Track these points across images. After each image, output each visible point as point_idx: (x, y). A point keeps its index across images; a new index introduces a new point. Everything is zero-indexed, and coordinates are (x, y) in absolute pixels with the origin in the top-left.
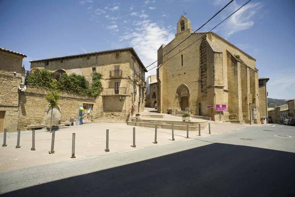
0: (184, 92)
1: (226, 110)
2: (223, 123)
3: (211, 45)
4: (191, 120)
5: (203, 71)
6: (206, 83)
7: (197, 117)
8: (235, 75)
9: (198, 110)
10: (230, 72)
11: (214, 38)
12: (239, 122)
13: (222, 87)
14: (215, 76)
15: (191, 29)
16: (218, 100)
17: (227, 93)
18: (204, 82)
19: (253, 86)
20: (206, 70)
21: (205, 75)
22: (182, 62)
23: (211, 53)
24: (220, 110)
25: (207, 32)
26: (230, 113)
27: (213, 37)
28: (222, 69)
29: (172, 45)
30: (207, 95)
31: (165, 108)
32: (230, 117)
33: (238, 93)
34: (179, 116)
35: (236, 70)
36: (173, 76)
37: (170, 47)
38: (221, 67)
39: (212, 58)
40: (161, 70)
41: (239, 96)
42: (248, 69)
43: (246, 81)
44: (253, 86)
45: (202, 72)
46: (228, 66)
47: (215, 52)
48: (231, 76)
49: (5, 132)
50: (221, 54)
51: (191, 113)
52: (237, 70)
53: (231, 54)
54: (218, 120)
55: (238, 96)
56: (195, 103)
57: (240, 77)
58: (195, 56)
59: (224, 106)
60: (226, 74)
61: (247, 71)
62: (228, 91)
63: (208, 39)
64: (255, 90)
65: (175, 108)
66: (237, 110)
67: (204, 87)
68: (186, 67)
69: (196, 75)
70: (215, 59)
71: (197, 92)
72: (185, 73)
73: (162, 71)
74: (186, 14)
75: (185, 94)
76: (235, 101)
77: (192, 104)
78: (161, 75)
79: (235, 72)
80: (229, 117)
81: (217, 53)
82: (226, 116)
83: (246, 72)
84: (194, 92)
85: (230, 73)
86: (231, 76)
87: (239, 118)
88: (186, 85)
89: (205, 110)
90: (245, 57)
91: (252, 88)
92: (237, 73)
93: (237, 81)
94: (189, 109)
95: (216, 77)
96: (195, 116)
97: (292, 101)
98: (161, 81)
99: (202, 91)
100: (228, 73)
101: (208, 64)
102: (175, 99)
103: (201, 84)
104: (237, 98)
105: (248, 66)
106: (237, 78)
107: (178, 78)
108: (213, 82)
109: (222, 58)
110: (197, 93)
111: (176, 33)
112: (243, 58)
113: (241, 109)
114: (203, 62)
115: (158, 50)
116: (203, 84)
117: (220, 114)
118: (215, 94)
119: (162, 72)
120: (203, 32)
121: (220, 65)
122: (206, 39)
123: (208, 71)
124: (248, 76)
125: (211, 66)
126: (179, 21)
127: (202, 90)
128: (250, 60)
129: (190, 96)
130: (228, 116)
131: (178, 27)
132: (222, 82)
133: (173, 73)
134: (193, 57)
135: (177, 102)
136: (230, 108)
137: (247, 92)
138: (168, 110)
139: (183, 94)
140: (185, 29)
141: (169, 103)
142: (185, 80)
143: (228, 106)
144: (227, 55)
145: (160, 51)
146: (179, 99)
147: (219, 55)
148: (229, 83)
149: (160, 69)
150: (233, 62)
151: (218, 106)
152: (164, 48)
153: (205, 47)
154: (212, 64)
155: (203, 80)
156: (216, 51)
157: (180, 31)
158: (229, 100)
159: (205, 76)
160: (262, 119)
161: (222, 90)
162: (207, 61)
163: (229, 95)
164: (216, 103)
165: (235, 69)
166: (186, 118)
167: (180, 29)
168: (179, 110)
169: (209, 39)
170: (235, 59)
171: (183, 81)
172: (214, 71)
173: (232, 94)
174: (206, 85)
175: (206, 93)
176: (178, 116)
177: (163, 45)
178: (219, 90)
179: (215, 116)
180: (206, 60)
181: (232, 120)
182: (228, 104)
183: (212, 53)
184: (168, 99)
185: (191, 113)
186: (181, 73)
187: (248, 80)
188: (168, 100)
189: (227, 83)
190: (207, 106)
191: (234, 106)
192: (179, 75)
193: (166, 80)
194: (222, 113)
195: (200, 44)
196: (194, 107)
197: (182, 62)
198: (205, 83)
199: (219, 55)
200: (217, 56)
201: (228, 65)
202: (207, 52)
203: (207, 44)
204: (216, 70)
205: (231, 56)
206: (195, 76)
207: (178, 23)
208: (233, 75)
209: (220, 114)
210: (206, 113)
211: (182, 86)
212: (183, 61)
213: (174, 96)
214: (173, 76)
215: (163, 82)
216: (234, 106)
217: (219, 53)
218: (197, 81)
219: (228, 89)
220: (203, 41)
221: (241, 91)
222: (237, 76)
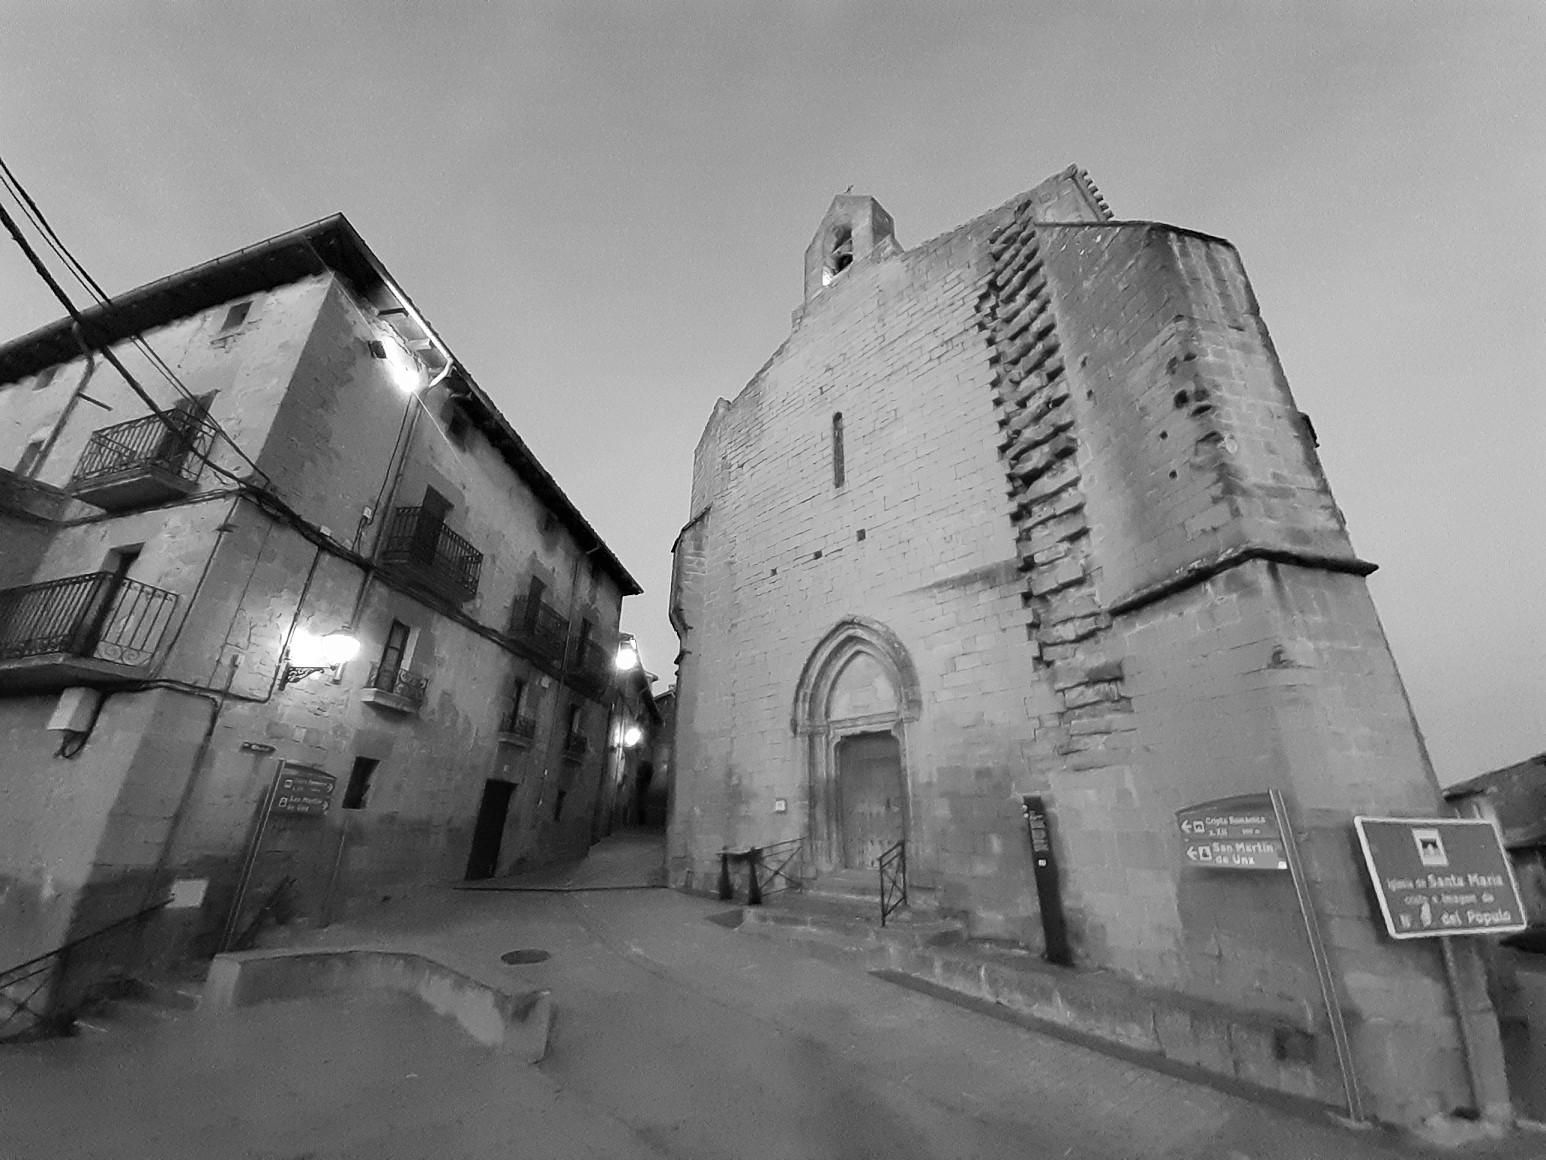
192: (818, 555)
200: (1191, 273)
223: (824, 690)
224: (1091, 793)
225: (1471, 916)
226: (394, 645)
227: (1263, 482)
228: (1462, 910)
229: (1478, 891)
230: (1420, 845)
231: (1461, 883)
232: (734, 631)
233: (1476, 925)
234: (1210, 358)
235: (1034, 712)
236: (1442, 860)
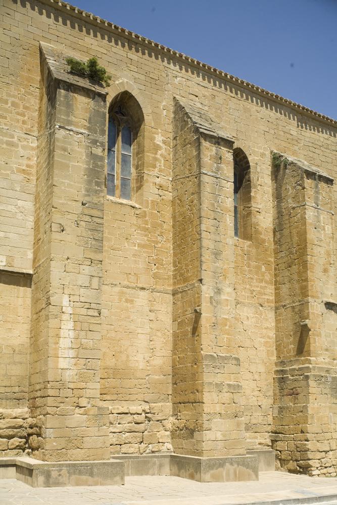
64: (306, 280)
91: (295, 268)
137: (201, 280)
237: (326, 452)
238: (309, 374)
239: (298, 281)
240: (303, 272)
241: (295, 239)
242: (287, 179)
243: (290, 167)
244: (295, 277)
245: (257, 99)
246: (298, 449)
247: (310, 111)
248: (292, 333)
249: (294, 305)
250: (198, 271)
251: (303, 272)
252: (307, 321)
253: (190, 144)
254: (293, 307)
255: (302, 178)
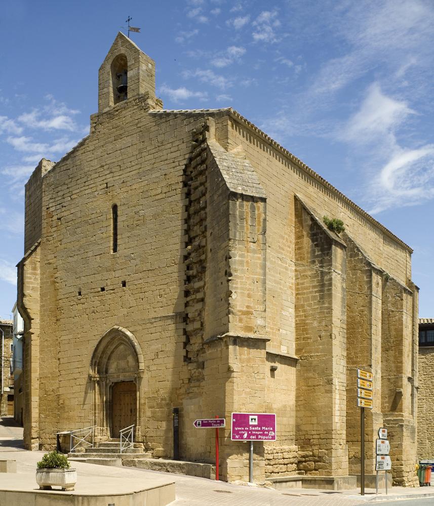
0: (123, 364)
1: (273, 438)
2: (262, 490)
3: (222, 165)
4: (72, 485)
5: (191, 272)
6: (202, 324)
7: (164, 464)
8: (322, 297)
9: (171, 434)
10: (306, 285)
11: (241, 137)
12: (330, 482)
13: (258, 343)
14: (234, 296)
15: (152, 94)
16: (244, 395)
17: (294, 369)
18: (194, 320)
19: (392, 345)
20: (204, 269)
21: (197, 291)
22: (115, 234)
23: (221, 198)
24: (248, 437)
25: (211, 110)
26: (302, 448)
27: (234, 133)
28: (264, 267)
29: (78, 163)
30: (206, 372)
31: (50, 428)
32: (301, 465)
33: (332, 369)
34: (95, 462)
35: (326, 278)
36: (80, 294)
37: (70, 172)
38: (259, 258)
39: (225, 217)
40: (35, 269)
41: (336, 381)
42: (376, 279)
43: (366, 326)
44: (392, 345)
45: (189, 279)
46: (297, 260)
47: (234, 195)
48: (306, 300)
49: (363, 456)
50: (261, 205)
51: (146, 450)
52: (331, 279)
53: (309, 214)
54: (241, 477)
55: (330, 382)
56: (160, 406)
57: (343, 306)
58: (163, 211)
59: (267, 420)
60: (289, 292)
61: (374, 286)
62: (296, 361)
63: (212, 142)
64: (401, 362)
65: (87, 430)
66: (327, 436)
67: (196, 342)
68: (129, 258)
69: (167, 291)
70: (236, 224)
71: (169, 362)
72: (124, 284)
73: (39, 272)
74: (137, 30)
75: (124, 370)
76: (321, 402)
77: (149, 414)
78: (33, 289)
79: (323, 285)
80: (300, 462)
81: (244, 197)
82: (286, 461)
83: (370, 288)
84: (157, 361)
85: (306, 288)
86: (306, 300)
87: (334, 466)
88: (128, 333)
89: (196, 437)
90: (372, 235)
91: (391, 353)
92: (330, 290)
93: (331, 320)
94: (139, 434)
95: (238, 301)
96: (161, 460)
97: (202, 366)
98: (32, 316)
99: (187, 359)
100: (297, 289)
101: (209, 247)
102: (86, 393)
103: (184, 329)
104: (328, 387)
105: (378, 267)
106: (330, 309)
107: (97, 303)
108: (223, 322)
109: (265, 220)
110: (170, 365)
111: (95, 111)
112: (354, 229)
113: (345, 432)
114: (194, 238)
115: (26, 186)
116: (190, 328)
117: (249, 451)
118: (229, 370)
119: (38, 277)
120: (198, 111)
121: (254, 252)
122: (204, 140)
123: (208, 277)
124: (374, 306)
125: (221, 253)
126: (107, 59)
127: (187, 352)
128: (390, 250)
129: (140, 378)
130: (292, 460)
131: (102, 86)
132: (260, 322)
133: (78, 282)
134: (156, 216)
135: (92, 402)
136: (303, 428)
137: (371, 366)
138: (58, 437)
139: (117, 370)
140: (129, 95)
141: (61, 407)
142: (125, 311)
143: (296, 422)
144: (298, 215)
145: (33, 188)
146: (104, 390)
147: (253, 209)
148: (301, 328)
149: (31, 263)
150: (316, 245)
151: (241, 420)
152: (46, 176)
153: (201, 173)
154: (224, 245)
155: (192, 312)
156: (239, 190)
157: (112, 104)
158: (297, 397)
159: (199, 296)
160: (426, 469)
161: (262, 353)
162: (208, 234)
163: (299, 376)
164: (236, 406)
165: (322, 272)
166: (51, 474)
167: (112, 95)
168: (103, 436)
169: (219, 140)
170: (324, 232)
171: (120, 314)
172: (231, 275)
173: (310, 375)
174: (203, 337)
175: (202, 366)
176: (89, 461)
177: (44, 163)
178: (246, 352)
179: (228, 461)
180: (203, 228)
181: (308, 476)
182: (297, 411)
183: (223, 200)
184: (61, 391)
185: (146, 450)
186: (109, 282)
187: (373, 322)
188: (58, 396)
189: (294, 330)
190: (199, 421)
191: (314, 420)
192: (103, 289)
193: (54, 313)
194: (259, 449)
195: (185, 162)
196: (156, 424)
197: (115, 234)
198: (197, 325)
199: (253, 209)
200: (242, 213)
201: (299, 257)
202: (208, 195)
203: (208, 162)
204: (236, 271)
205: (310, 223)
206: (161, 296)
207: (102, 68)
208: (314, 298)
209: (249, 451)
210: (201, 450)
211: (113, 339)
212: (119, 232)
213: (84, 381)
214: (80, 294)
215: (42, 320)
216: (314, 420)
217: (253, 199)
218: (172, 317)
219: (296, 354)
220: (194, 147)
221: (343, 362)
222: (330, 303)
223: (105, 361)
224: (192, 406)
225: (259, 437)
226: (19, 363)
227: (242, 309)
228: (257, 435)
229: (264, 431)
230: (250, 420)
231: (260, 429)
232: (59, 323)
233: (260, 439)
234: (237, 258)
235: (182, 377)
236: (256, 423)
237: (408, 472)
238: (403, 424)
239: (394, 362)
240: (399, 357)
241: (393, 333)
242: (388, 289)
243: (390, 281)
244: (392, 359)
245: (364, 220)
246: (395, 471)
247: (248, 122)
248: (387, 396)
249: (390, 377)
250: (368, 359)
251: (399, 357)
252: (402, 390)
253: (361, 271)
254: (389, 379)
255: (401, 292)
